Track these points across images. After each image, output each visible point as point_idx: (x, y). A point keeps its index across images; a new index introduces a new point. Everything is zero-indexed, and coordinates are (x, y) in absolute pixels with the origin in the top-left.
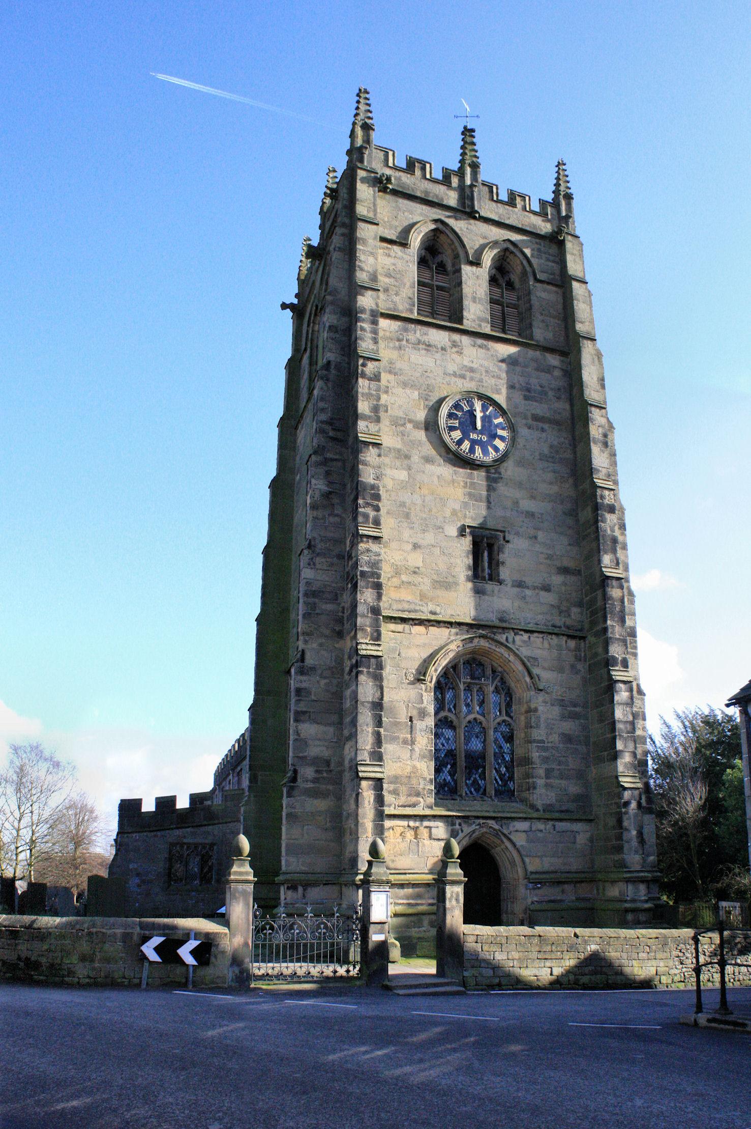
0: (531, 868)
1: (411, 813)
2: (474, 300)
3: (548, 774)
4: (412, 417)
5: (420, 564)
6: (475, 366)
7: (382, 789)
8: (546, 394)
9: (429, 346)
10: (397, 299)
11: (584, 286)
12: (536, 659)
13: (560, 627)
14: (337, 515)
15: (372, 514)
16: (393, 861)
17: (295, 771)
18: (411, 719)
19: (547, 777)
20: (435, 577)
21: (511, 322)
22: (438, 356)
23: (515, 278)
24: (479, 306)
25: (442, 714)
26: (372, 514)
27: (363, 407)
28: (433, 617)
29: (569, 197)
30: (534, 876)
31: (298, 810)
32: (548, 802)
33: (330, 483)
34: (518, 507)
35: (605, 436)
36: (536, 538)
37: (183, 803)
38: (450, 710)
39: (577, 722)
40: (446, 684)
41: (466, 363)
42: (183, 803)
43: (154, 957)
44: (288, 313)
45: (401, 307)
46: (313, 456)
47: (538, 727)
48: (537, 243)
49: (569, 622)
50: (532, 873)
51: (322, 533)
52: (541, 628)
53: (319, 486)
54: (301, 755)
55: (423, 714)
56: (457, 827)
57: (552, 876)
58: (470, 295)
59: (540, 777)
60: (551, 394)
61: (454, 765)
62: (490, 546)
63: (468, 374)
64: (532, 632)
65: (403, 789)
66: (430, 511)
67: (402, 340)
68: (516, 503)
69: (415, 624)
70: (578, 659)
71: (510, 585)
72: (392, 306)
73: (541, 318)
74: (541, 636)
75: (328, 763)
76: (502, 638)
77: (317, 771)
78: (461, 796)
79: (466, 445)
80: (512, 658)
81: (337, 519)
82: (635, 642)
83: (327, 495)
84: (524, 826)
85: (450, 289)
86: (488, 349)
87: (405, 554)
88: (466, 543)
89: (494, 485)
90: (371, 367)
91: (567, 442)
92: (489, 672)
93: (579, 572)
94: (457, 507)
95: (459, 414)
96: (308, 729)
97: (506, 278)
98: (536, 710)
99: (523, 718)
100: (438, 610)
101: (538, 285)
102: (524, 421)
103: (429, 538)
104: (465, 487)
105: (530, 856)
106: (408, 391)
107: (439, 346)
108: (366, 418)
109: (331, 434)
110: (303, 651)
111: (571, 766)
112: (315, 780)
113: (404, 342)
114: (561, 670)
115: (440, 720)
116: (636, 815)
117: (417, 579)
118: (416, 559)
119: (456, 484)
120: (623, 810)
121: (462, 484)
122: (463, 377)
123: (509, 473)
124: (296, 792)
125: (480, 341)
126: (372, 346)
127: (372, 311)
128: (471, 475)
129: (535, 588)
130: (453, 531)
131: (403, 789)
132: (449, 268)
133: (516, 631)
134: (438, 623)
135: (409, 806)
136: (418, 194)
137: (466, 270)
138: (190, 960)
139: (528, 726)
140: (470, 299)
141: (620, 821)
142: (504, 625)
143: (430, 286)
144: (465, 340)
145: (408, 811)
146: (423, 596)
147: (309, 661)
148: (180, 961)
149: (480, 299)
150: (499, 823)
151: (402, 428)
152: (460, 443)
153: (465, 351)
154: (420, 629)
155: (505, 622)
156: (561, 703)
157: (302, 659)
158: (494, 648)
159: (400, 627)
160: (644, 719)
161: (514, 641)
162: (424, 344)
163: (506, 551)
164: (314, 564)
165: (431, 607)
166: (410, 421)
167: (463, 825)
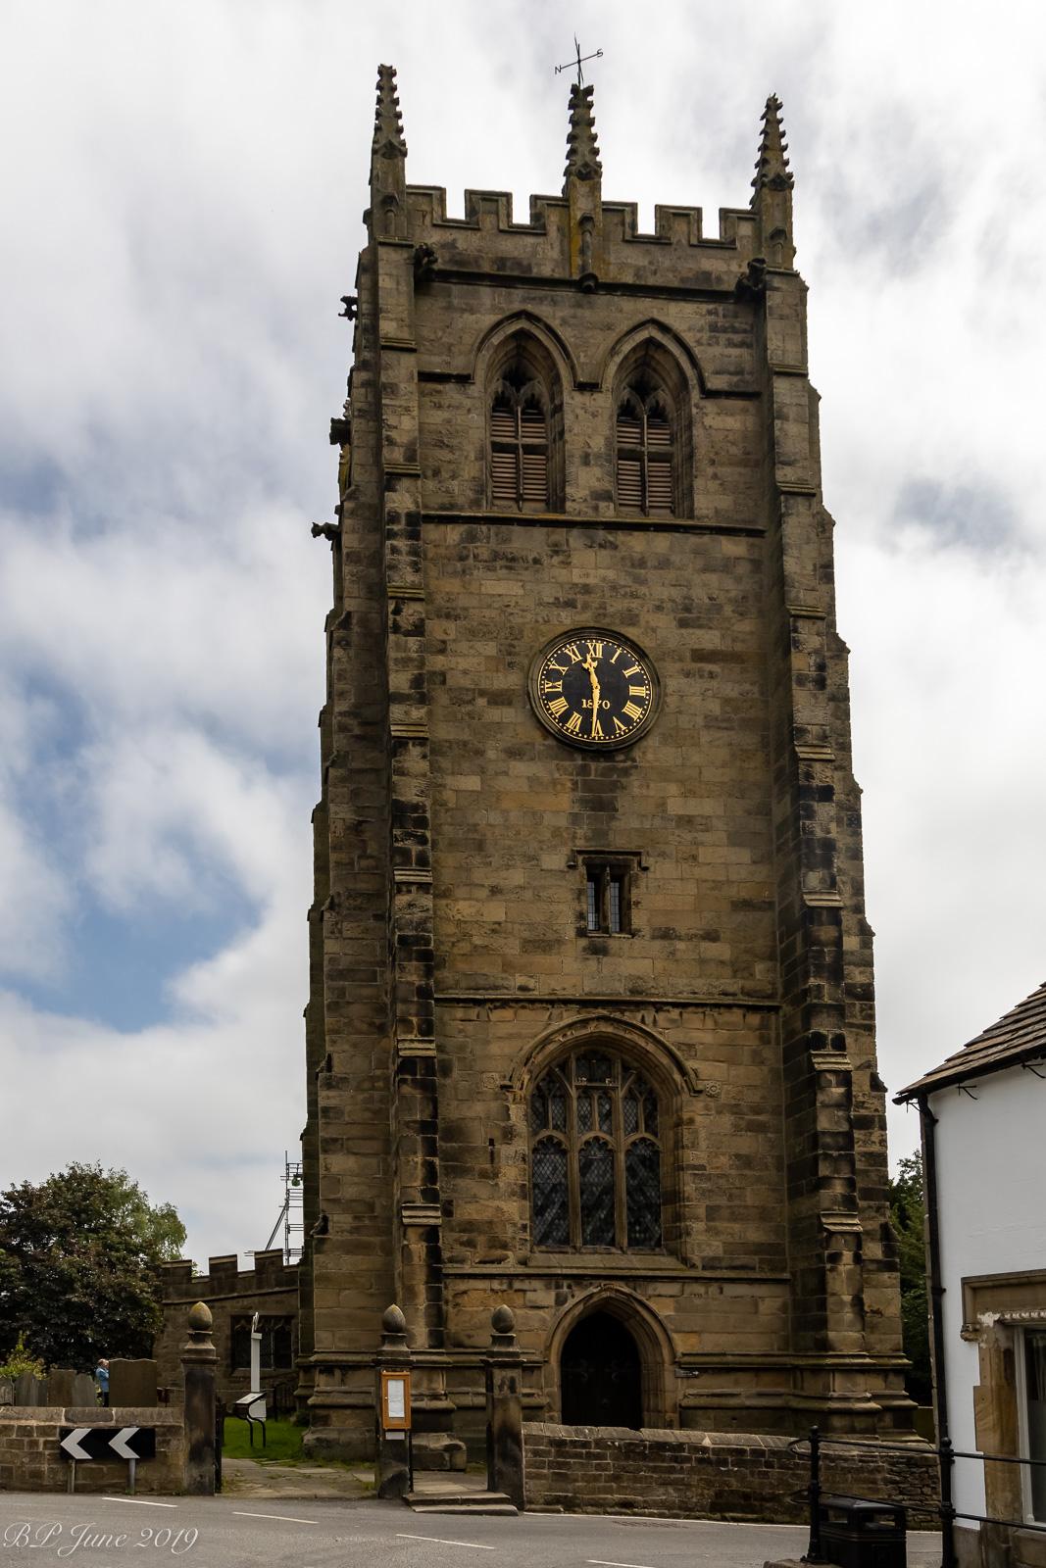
1: (494, 1271)
2: (586, 460)
3: (712, 1213)
4: (484, 685)
5: (502, 917)
6: (591, 581)
8: (719, 608)
9: (513, 559)
10: (454, 485)
11: (798, 383)
12: (691, 1046)
13: (734, 995)
14: (372, 857)
15: (415, 849)
16: (469, 1337)
17: (325, 1219)
18: (492, 1142)
20: (526, 934)
21: (659, 489)
22: (527, 575)
24: (597, 471)
25: (544, 1133)
26: (415, 849)
27: (399, 681)
28: (521, 995)
30: (686, 1359)
32: (711, 1254)
33: (359, 810)
34: (665, 811)
35: (821, 667)
36: (694, 858)
38: (556, 1127)
39: (761, 1137)
40: (550, 1090)
41: (576, 580)
43: (80, 1454)
44: (324, 544)
45: (461, 500)
46: (331, 770)
47: (694, 1146)
48: (710, 313)
49: (749, 984)
50: (684, 1355)
51: (351, 886)
52: (701, 998)
53: (341, 816)
54: (332, 1197)
55: (509, 1134)
56: (565, 1289)
57: (716, 1359)
58: (578, 453)
59: (697, 1219)
60: (728, 610)
63: (580, 599)
64: (684, 1005)
65: (481, 1240)
66: (518, 833)
67: (467, 557)
69: (496, 1008)
70: (765, 1040)
71: (647, 937)
72: (446, 500)
73: (710, 471)
74: (700, 1010)
75: (371, 1207)
76: (627, 1017)
77: (355, 1218)
78: (574, 1247)
79: (575, 721)
80: (650, 1047)
81: (371, 862)
82: (872, 1008)
84: (673, 1289)
85: (546, 446)
86: (615, 547)
87: (479, 904)
88: (578, 878)
89: (623, 780)
90: (411, 612)
91: (756, 689)
92: (618, 1068)
93: (769, 905)
94: (563, 822)
95: (564, 669)
97: (650, 401)
98: (691, 1121)
99: (671, 1134)
100: (531, 983)
101: (710, 406)
102: (678, 665)
103: (517, 877)
104: (574, 789)
105: (680, 1332)
106: (479, 645)
107: (530, 558)
108: (400, 698)
110: (329, 1056)
111: (749, 1203)
112: (355, 1230)
113: (471, 561)
114: (732, 1061)
115: (540, 1142)
116: (850, 1273)
117: (497, 942)
118: (496, 911)
119: (559, 787)
120: (828, 1266)
121: (569, 784)
122: (570, 604)
123: (650, 756)
124: (326, 1247)
125: (601, 534)
126: (410, 577)
127: (409, 515)
129: (691, 938)
130: (556, 860)
131: (481, 1240)
132: (547, 407)
133: (658, 1007)
134: (566, 1002)
135: (492, 1262)
136: (486, 268)
137: (573, 401)
138: (128, 1453)
140: (577, 460)
142: (638, 999)
143: (511, 449)
144: (576, 539)
146: (508, 967)
147: (338, 1069)
148: (114, 1455)
149: (598, 456)
150: (632, 1284)
151: (469, 708)
152: (565, 717)
153: (575, 560)
154: (508, 1013)
155: (640, 993)
156: (735, 1109)
157: (329, 1068)
158: (622, 1033)
159: (473, 1013)
160: (883, 1127)
161: (655, 1021)
162: (505, 557)
163: (643, 884)
164: (340, 932)
165: (520, 980)
166: (482, 693)
167: (574, 1288)
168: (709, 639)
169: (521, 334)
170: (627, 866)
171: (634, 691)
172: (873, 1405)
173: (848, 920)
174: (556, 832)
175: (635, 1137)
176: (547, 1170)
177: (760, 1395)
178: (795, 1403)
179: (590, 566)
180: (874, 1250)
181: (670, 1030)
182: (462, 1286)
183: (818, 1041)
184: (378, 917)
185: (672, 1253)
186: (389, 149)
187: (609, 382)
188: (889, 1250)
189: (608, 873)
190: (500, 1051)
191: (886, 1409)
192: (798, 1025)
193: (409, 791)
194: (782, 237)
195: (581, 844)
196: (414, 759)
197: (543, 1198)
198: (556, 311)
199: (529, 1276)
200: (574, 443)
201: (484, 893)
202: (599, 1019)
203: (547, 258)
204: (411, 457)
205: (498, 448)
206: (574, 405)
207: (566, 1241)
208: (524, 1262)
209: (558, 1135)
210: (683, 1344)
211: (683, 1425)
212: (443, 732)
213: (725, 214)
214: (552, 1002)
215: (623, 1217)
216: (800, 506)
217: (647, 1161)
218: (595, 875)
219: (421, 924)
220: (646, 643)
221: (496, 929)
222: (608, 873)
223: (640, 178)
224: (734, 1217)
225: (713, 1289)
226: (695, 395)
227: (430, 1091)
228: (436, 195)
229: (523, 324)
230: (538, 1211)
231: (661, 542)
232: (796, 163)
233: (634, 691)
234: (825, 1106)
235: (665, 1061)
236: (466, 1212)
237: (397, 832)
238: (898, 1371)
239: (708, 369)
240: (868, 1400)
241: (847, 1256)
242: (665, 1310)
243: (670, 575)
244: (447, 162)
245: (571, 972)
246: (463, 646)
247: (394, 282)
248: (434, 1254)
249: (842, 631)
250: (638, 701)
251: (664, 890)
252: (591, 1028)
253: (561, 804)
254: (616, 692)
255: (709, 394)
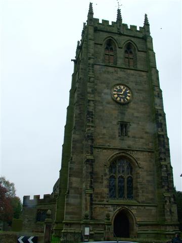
0: (138, 220)
5: (105, 132)
7: (92, 196)
17: (69, 191)
18: (102, 176)
19: (143, 193)
23: (132, 50)
25: (112, 174)
29: (148, 25)
31: (69, 202)
33: (80, 111)
37: (42, 197)
42: (42, 197)
44: (73, 62)
55: (106, 175)
61: (115, 189)
62: (126, 127)
65: (99, 196)
68: (133, 114)
76: (127, 152)
83: (80, 114)
84: (136, 207)
88: (119, 126)
94: (116, 116)
96: (74, 179)
98: (139, 173)
101: (139, 52)
109: (81, 97)
122: (118, 80)
123: (131, 105)
125: (123, 70)
128: (120, 107)
129: (138, 138)
130: (115, 122)
131: (99, 196)
133: (133, 151)
134: (116, 149)
139: (137, 178)
141: (164, 206)
145: (101, 203)
152: (117, 98)
154: (105, 151)
157: (72, 159)
165: (108, 144)
168: (140, 88)
169: (110, 40)
170: (127, 124)
171: (128, 95)
172: (174, 233)
173: (165, 136)
174: (115, 118)
175: (128, 176)
176: (112, 182)
177: (153, 230)
178: (159, 232)
179: (121, 74)
180: (172, 200)
181: (136, 155)
182: (95, 206)
183: (161, 159)
184: (83, 131)
185: (136, 200)
186: (91, 13)
187: (123, 47)
188: (175, 200)
189: (124, 126)
190: (104, 157)
191: (176, 233)
192: (158, 155)
193: (91, 109)
194: (148, 31)
195: (119, 120)
196: (92, 104)
197: (111, 188)
198: (116, 37)
199: (108, 204)
200: (118, 55)
201: (102, 128)
202: (123, 152)
203: (115, 30)
204: (93, 55)
205: (106, 54)
206: (114, 60)
207: (115, 197)
208: (107, 202)
209: (114, 175)
210: (138, 219)
211: (138, 237)
212: (97, 98)
213: (140, 27)
214: (114, 149)
215: (126, 192)
216: (153, 69)
217: (130, 181)
218: (122, 125)
219: (91, 133)
220: (131, 87)
221: (104, 134)
222: (124, 126)
223: (127, 21)
224: (147, 193)
225: (143, 208)
226: (137, 51)
227: (92, 165)
228: (98, 20)
229: (110, 38)
230: (110, 191)
231: (132, 72)
232: (150, 22)
233: (128, 95)
234: (163, 171)
235: (134, 161)
236: (97, 190)
237: (88, 116)
238: (177, 225)
239: (138, 47)
240: (173, 231)
241: (168, 201)
242: (134, 212)
243: (134, 77)
244: (99, 15)
245: (117, 143)
246: (100, 84)
247: (91, 31)
248: (91, 199)
249: (161, 88)
250: (129, 96)
251: (133, 129)
252: (121, 154)
253: (116, 113)
254: (125, 94)
255: (139, 51)
